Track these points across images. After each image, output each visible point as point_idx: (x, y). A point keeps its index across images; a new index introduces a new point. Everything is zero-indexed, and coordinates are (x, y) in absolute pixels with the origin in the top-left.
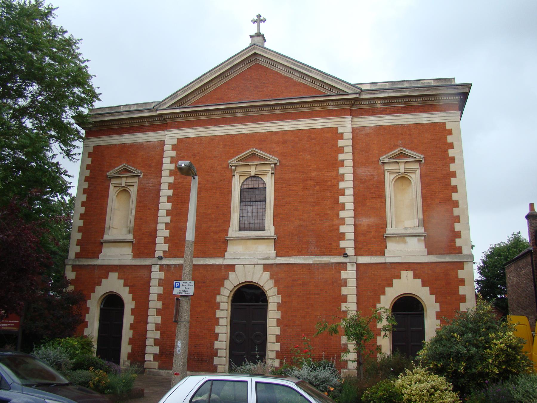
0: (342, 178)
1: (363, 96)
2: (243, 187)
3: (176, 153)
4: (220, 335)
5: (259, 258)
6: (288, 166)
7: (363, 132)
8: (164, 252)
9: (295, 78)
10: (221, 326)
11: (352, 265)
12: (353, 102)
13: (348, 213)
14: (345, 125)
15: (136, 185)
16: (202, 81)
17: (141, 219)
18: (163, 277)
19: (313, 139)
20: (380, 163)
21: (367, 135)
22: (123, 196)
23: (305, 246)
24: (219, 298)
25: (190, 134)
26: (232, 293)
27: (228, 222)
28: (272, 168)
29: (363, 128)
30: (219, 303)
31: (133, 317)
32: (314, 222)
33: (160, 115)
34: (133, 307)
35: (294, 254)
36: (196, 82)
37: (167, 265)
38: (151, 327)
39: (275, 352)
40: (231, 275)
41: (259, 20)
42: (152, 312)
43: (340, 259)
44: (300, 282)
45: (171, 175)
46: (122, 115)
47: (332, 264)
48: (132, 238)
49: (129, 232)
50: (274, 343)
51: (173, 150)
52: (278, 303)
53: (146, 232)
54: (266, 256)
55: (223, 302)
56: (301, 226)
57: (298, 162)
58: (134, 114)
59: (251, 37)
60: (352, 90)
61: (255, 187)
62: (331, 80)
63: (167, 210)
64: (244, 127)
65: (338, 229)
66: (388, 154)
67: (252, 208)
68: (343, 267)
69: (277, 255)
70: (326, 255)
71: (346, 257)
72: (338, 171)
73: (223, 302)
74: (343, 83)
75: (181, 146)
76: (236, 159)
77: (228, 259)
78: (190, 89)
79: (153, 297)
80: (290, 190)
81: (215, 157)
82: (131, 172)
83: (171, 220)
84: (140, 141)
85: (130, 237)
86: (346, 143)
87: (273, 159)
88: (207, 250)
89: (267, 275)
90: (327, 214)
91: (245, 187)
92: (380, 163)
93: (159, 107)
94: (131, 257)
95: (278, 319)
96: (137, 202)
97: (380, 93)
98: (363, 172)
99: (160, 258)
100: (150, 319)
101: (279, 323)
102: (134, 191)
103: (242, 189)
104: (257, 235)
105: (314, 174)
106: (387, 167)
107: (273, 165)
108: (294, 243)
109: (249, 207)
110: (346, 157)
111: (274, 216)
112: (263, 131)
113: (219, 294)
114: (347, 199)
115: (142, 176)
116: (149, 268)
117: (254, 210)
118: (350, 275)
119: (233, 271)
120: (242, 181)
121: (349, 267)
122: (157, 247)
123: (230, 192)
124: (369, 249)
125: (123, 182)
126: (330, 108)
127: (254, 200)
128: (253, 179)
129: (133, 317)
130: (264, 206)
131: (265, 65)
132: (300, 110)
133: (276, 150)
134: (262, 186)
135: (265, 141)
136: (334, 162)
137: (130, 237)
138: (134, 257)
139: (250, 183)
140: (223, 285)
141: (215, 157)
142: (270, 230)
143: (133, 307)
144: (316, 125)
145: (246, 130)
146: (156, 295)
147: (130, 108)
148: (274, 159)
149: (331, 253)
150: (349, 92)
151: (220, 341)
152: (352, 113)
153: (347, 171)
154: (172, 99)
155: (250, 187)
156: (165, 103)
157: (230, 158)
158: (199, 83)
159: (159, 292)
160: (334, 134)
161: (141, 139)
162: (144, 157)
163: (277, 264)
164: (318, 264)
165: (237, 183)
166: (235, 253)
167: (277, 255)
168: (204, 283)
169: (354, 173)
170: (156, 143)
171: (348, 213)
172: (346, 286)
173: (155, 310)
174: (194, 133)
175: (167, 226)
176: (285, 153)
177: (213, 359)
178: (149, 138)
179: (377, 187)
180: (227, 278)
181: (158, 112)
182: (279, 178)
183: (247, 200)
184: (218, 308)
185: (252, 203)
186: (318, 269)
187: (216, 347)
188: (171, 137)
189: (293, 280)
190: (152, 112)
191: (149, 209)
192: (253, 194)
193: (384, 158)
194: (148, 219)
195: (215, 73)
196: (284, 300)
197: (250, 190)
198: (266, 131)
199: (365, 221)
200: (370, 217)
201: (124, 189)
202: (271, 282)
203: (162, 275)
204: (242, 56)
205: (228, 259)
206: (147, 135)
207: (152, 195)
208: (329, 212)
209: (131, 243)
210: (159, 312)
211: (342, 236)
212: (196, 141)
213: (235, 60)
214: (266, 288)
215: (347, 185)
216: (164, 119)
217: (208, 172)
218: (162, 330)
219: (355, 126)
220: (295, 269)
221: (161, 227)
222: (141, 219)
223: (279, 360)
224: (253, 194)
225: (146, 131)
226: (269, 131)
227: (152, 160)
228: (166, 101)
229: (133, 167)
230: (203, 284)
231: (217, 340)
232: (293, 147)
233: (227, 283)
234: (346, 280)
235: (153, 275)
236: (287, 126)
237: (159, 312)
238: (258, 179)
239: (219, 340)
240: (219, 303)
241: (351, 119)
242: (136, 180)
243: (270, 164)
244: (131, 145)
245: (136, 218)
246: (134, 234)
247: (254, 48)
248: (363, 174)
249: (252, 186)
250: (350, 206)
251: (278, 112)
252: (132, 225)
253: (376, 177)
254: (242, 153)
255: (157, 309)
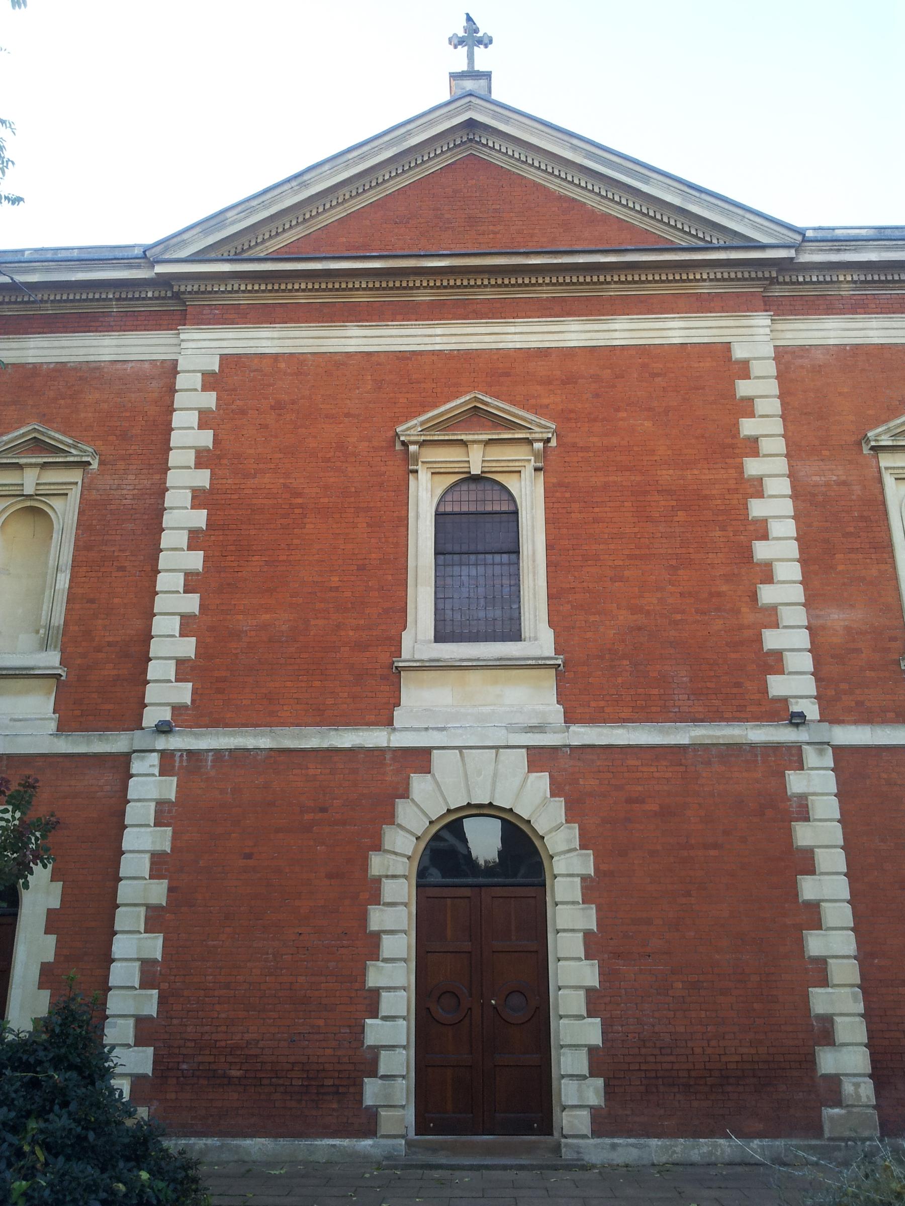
0: (757, 488)
1: (805, 258)
2: (441, 509)
3: (218, 399)
4: (384, 994)
5: (511, 728)
6: (585, 449)
7: (805, 362)
8: (177, 709)
9: (591, 201)
10: (386, 960)
11: (821, 752)
12: (774, 275)
13: (785, 590)
14: (755, 338)
15: (75, 494)
16: (305, 185)
17: (92, 601)
18: (171, 794)
19: (658, 375)
20: (866, 451)
21: (817, 370)
22: (22, 530)
23: (656, 691)
24: (377, 864)
25: (265, 343)
26: (422, 845)
27: (398, 614)
28: (536, 455)
29: (804, 350)
30: (378, 880)
31: (52, 939)
32: (679, 617)
33: (165, 281)
34: (56, 904)
35: (622, 715)
36: (286, 187)
37: (190, 752)
38: (123, 973)
39: (585, 1051)
40: (419, 784)
41: (472, 37)
42: (128, 918)
43: (784, 734)
44: (652, 806)
45: (199, 465)
46: (34, 271)
47: (753, 746)
48: (57, 663)
49: (45, 645)
50: (581, 1017)
51: (205, 388)
52: (584, 878)
53: (110, 644)
54: (534, 722)
55: (394, 877)
56: (639, 629)
57: (615, 440)
58: (71, 270)
59: (454, 76)
60: (776, 237)
61: (480, 509)
62: (711, 207)
63: (188, 574)
64: (439, 331)
65: (759, 640)
66: (892, 424)
67: (473, 572)
68: (792, 757)
69: (570, 719)
70: (727, 720)
71: (797, 725)
72: (740, 468)
73: (394, 877)
74: (748, 215)
75: (228, 376)
76: (422, 423)
77: (406, 729)
78: (267, 207)
79: (135, 864)
80: (596, 521)
81: (347, 415)
82: (57, 450)
83: (202, 606)
84: (92, 358)
85: (51, 660)
86: (761, 387)
87: (540, 426)
88: (330, 701)
89: (541, 781)
90: (719, 594)
91: (449, 509)
92: (866, 451)
93: (167, 249)
94: (53, 726)
95: (587, 934)
96: (77, 548)
97: (856, 250)
98: (819, 474)
99: (163, 729)
100: (122, 946)
101: (593, 946)
102: (65, 512)
103: (438, 515)
104: (497, 655)
105: (666, 475)
106: (886, 461)
107: (539, 446)
108: (620, 680)
109: (465, 570)
110: (765, 425)
111: (550, 597)
112: (501, 346)
113: (378, 847)
114: (780, 548)
115: (95, 465)
116: (120, 765)
117: (481, 581)
118: (815, 782)
119: (426, 769)
120: (439, 492)
121: (811, 757)
122: (152, 693)
123: (404, 521)
124: (859, 704)
125: (29, 481)
126: (705, 289)
127: (480, 548)
128: (473, 486)
129: (52, 939)
130: (513, 568)
131: (497, 160)
132: (613, 291)
133: (546, 401)
134: (505, 508)
135: (507, 375)
136: (729, 441)
137: (51, 660)
138: (63, 728)
139: (464, 498)
140: (390, 818)
141: (347, 415)
142: (539, 638)
143: (56, 904)
144: (664, 333)
145: (445, 339)
146: (147, 857)
147: (23, 255)
148: (542, 427)
149: (740, 715)
150: (765, 240)
151: (386, 1018)
152: (781, 308)
153: (770, 467)
154: (206, 232)
155: (465, 509)
156: (184, 244)
157: (408, 418)
158: (296, 193)
159: (158, 848)
160: (723, 364)
161: (92, 351)
162: (105, 406)
163: (573, 748)
164: (706, 747)
165: (425, 496)
166: (427, 710)
167: (570, 719)
168: (323, 810)
169: (792, 476)
170: (147, 365)
171: (785, 590)
172: (807, 819)
173: (143, 910)
174: (276, 342)
175: (188, 625)
176: (571, 411)
177: (361, 1085)
178: (120, 350)
179: (862, 518)
180: (405, 794)
181: (159, 269)
182: (560, 485)
183: (457, 548)
184: (376, 898)
185: (473, 557)
186: (709, 763)
187: (371, 1039)
188: (199, 349)
189: (630, 801)
190: (139, 267)
191: (122, 569)
192: (477, 531)
193: (879, 435)
194: (116, 600)
195: (347, 167)
196: (604, 867)
197: (464, 519)
198: (511, 345)
199: (837, 618)
200: (852, 606)
201: (28, 504)
202: (558, 806)
203: (169, 788)
204: (432, 123)
205: (406, 729)
206: (115, 342)
207: (130, 526)
208: (724, 588)
209: (53, 682)
210: (155, 919)
211: (775, 662)
212: (283, 365)
213: (409, 133)
214: (541, 826)
215: (775, 508)
216: (177, 296)
217: (328, 460)
218: (165, 986)
219: (779, 343)
220: (632, 762)
221: (165, 625)
222: (92, 601)
223: (600, 1082)
224: (477, 531)
225: (110, 329)
226: (518, 346)
227: (135, 419)
228: (185, 236)
229: (64, 433)
230: (319, 816)
231: (375, 1014)
232: (597, 396)
233: (404, 811)
234: (803, 799)
235: (135, 788)
236: (573, 333)
237: (155, 919)
238: (488, 487)
239: (383, 1012)
240: (378, 880)
241: (768, 322)
242: (76, 476)
243: (529, 442)
244: (55, 370)
245: (71, 598)
246: (62, 651)
247: (469, 107)
248: (817, 478)
249: (473, 509)
250: (789, 571)
251: (545, 294)
252: (58, 619)
253: (857, 490)
254: (436, 406)
255: (148, 907)
